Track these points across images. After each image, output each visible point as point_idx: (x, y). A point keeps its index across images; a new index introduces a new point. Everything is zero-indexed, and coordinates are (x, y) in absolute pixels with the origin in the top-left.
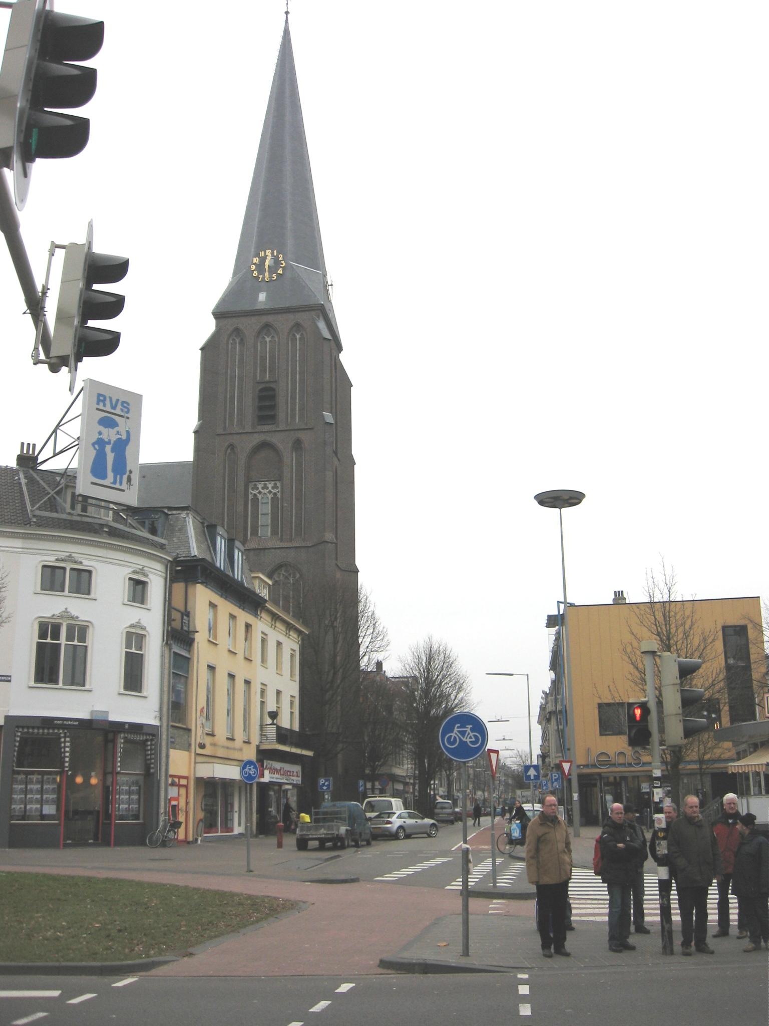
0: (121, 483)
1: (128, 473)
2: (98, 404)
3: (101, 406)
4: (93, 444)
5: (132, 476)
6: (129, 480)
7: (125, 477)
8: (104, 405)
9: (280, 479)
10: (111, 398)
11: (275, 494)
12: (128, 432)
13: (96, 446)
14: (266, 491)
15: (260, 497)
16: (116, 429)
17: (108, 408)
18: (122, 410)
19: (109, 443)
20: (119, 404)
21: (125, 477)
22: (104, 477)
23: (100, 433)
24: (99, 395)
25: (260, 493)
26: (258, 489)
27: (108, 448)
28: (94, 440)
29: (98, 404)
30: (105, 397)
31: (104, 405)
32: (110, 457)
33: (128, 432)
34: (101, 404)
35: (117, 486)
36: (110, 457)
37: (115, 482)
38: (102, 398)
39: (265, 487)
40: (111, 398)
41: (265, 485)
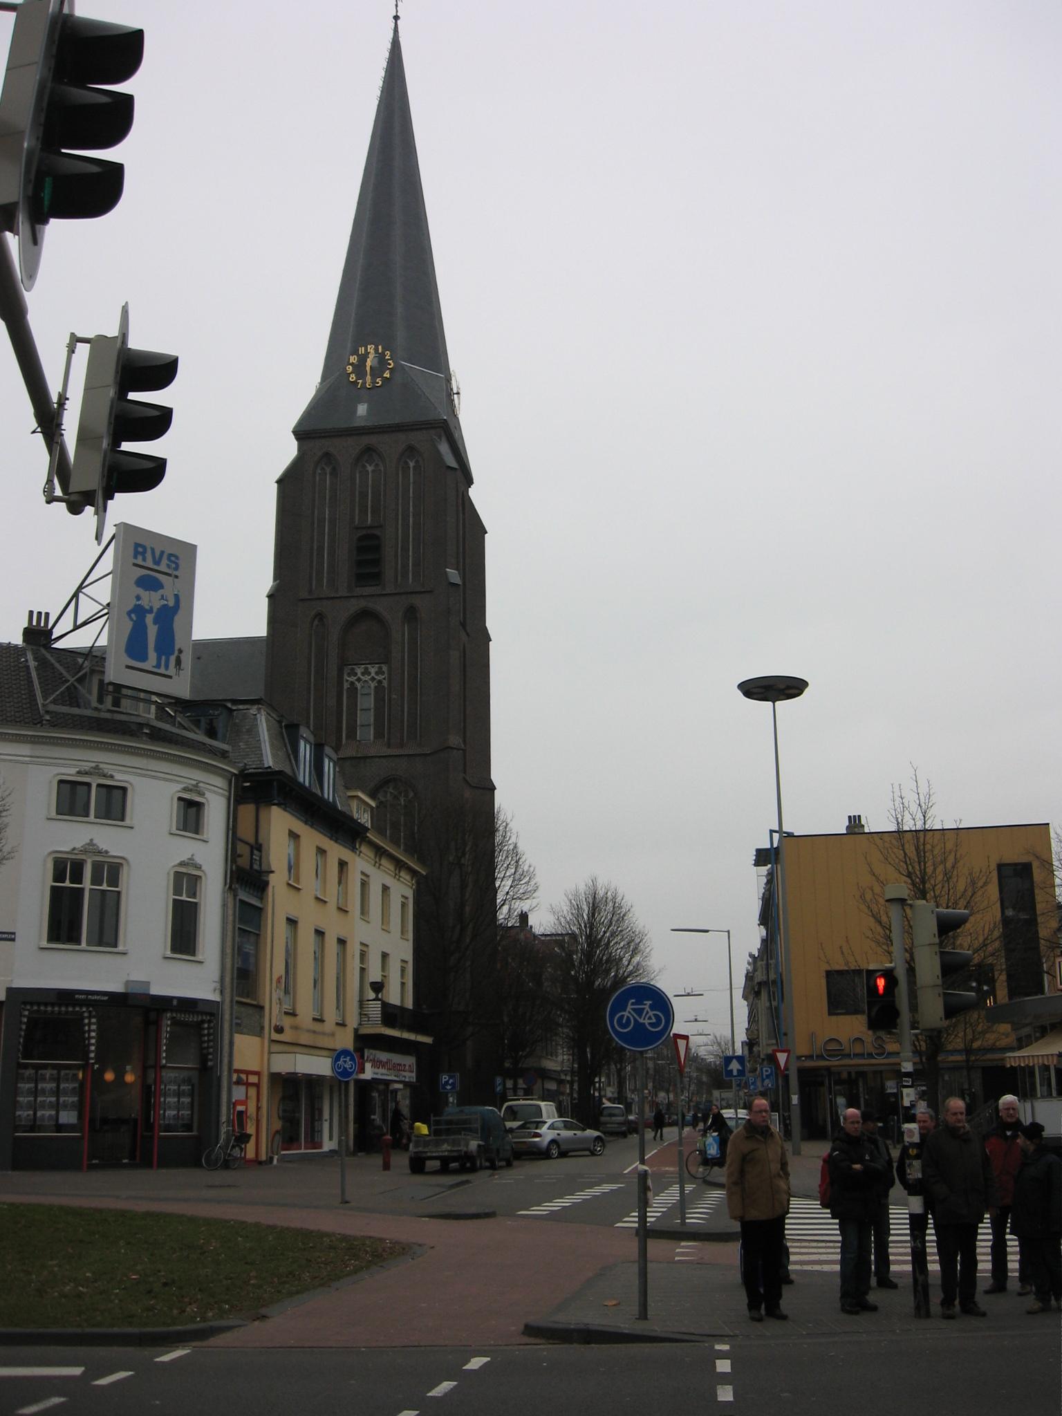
0: (167, 667)
1: (176, 653)
2: (135, 557)
3: (139, 561)
4: (129, 613)
5: (183, 657)
6: (178, 662)
7: (173, 659)
8: (144, 560)
9: (386, 660)
10: (153, 550)
11: (380, 682)
12: (177, 597)
13: (133, 616)
14: (367, 678)
15: (359, 685)
16: (161, 592)
17: (149, 563)
18: (168, 566)
19: (151, 611)
20: (165, 556)
21: (173, 659)
22: (144, 658)
23: (138, 598)
24: (137, 545)
25: (359, 680)
26: (369, 674)
27: (149, 619)
28: (130, 607)
29: (135, 557)
30: (144, 548)
31: (144, 560)
32: (152, 631)
33: (177, 597)
34: (140, 558)
35: (162, 671)
36: (152, 631)
37: (158, 666)
38: (140, 549)
39: (366, 672)
40: (153, 550)
41: (366, 669)
